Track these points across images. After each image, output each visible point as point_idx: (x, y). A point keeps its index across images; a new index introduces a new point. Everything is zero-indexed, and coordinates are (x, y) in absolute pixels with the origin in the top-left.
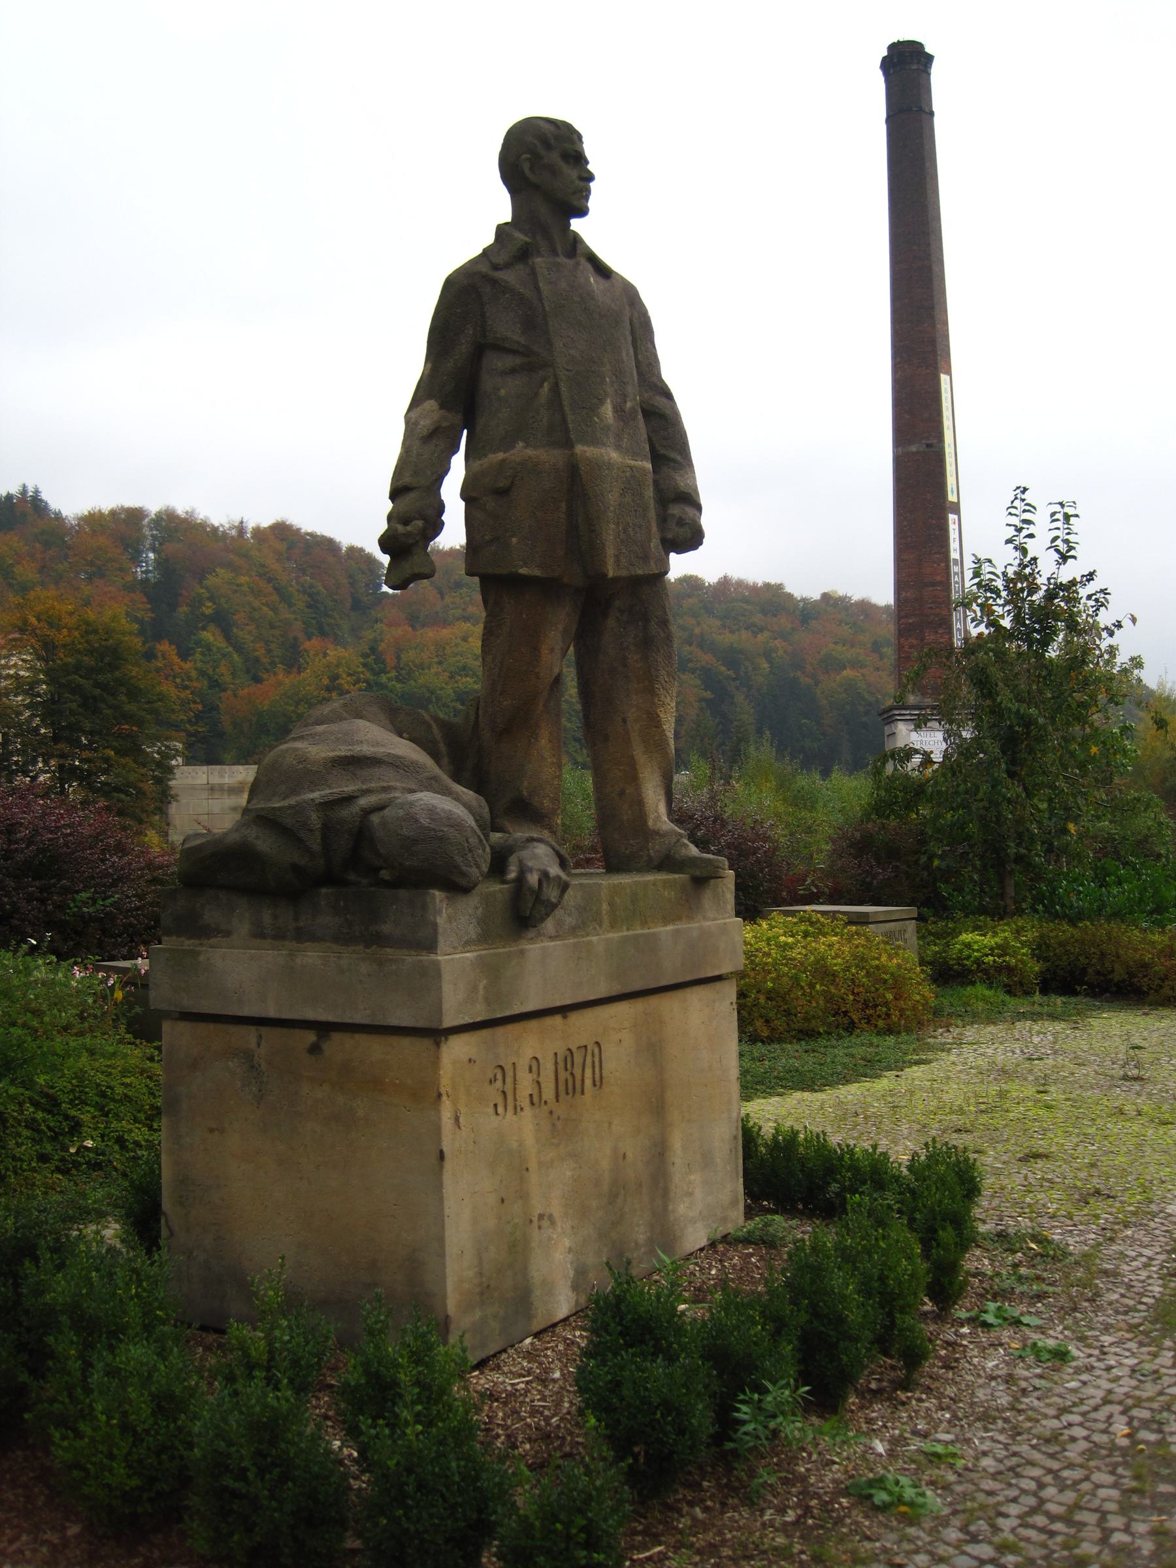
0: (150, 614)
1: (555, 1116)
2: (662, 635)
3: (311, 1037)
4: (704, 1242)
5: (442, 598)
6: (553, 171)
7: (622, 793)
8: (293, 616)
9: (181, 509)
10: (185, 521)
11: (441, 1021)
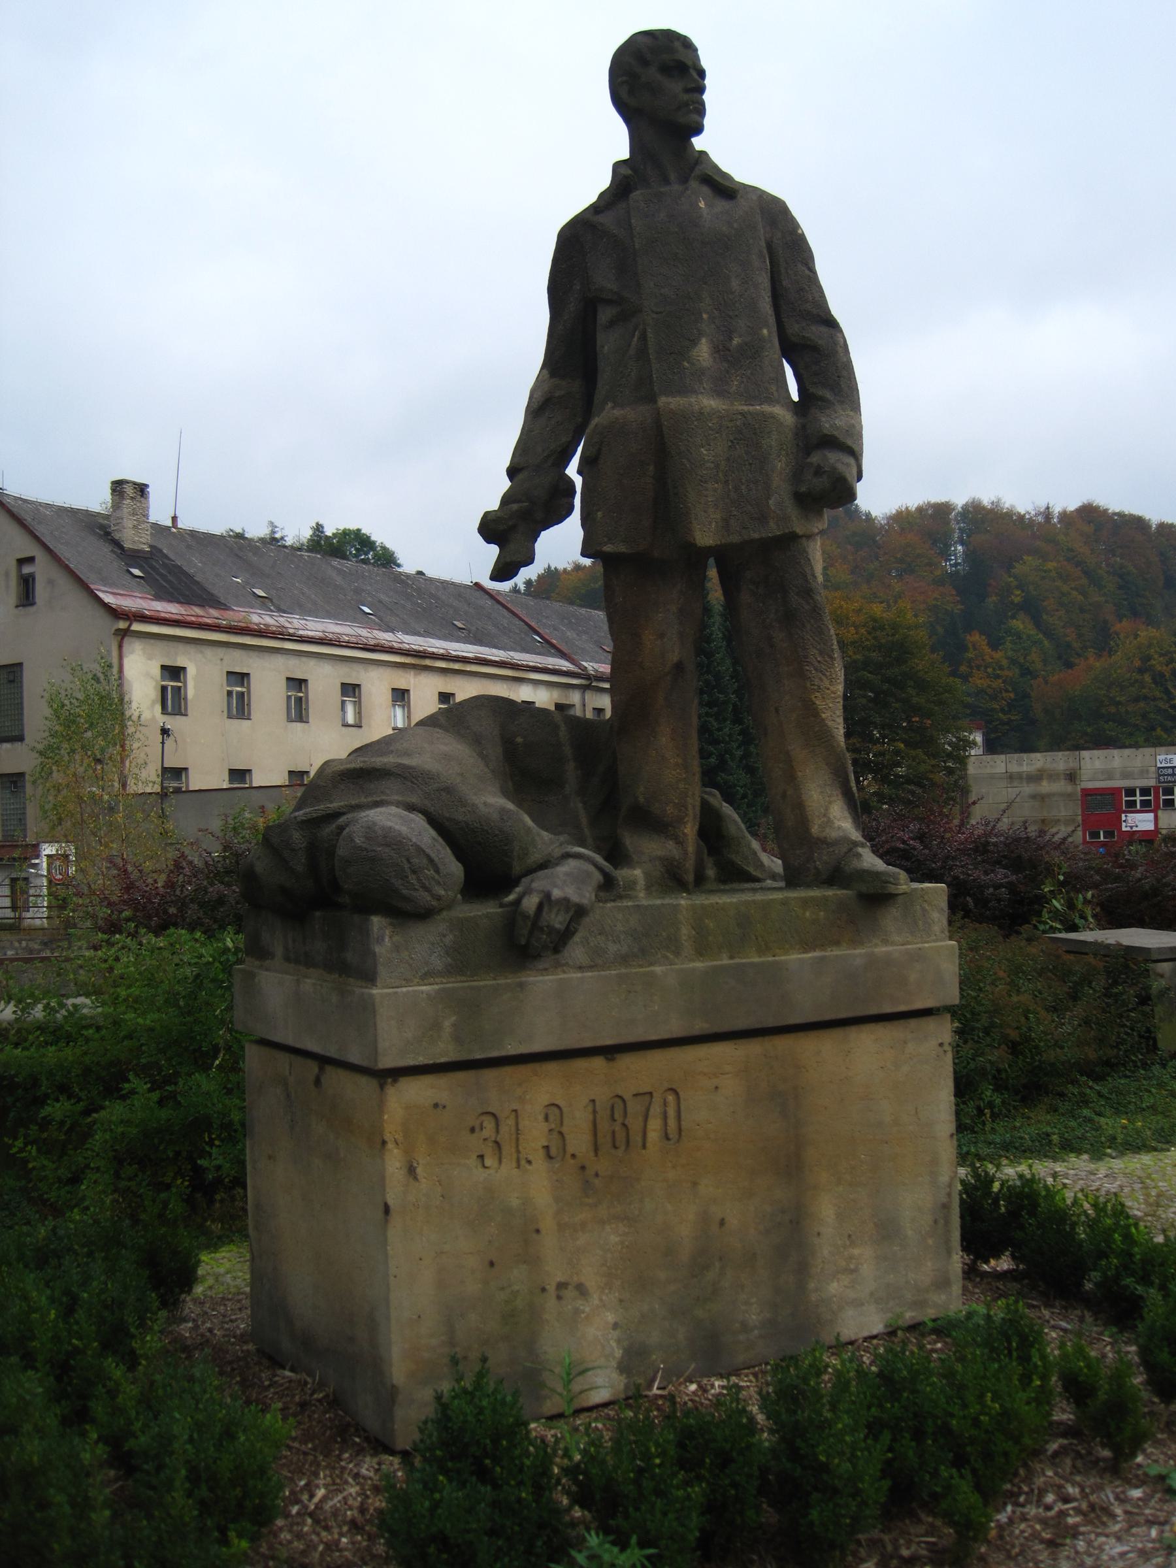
0: (959, 607)
2: (807, 607)
3: (313, 1067)
4: (878, 1328)
7: (784, 795)
8: (1103, 599)
9: (986, 500)
10: (992, 510)
11: (376, 1061)
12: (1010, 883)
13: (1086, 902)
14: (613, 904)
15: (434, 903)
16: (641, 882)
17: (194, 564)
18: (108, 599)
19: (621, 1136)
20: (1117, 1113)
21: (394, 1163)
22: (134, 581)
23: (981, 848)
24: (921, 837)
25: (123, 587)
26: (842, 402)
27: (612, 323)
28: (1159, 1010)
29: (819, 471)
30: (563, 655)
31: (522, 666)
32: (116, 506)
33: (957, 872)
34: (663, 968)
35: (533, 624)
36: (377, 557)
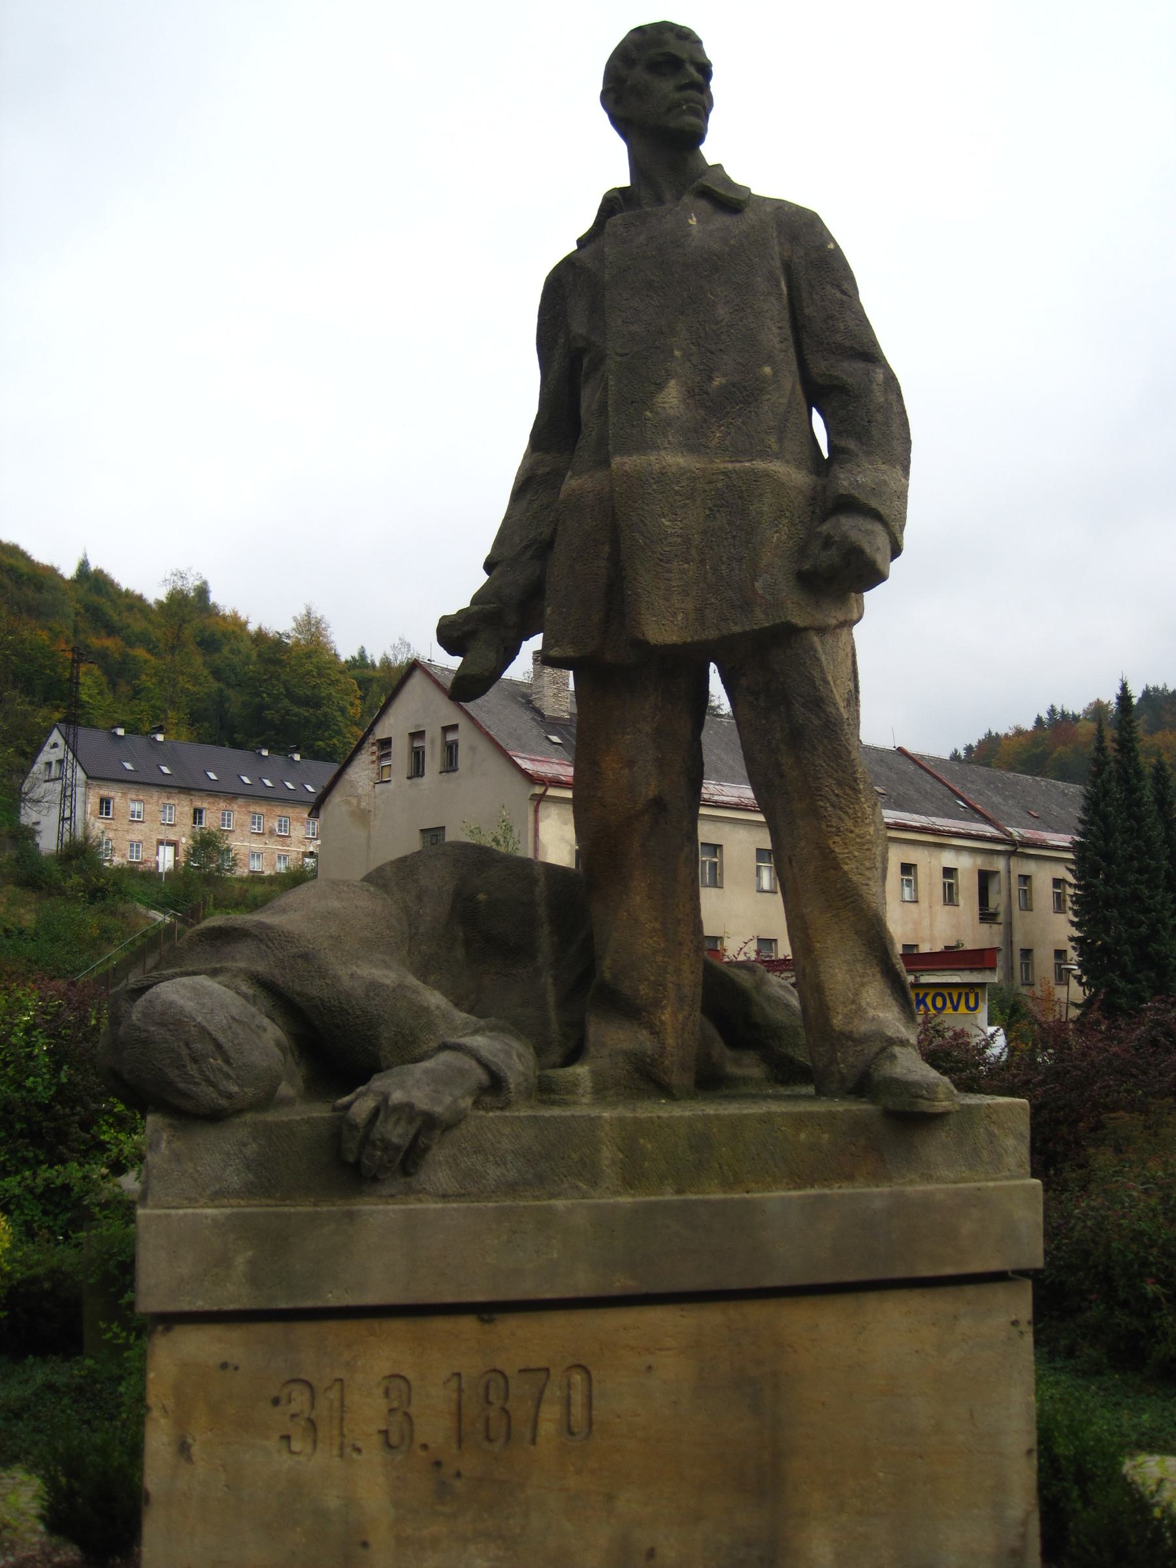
2: (816, 722)
14: (498, 1113)
15: (223, 1102)
18: (525, 765)
22: (552, 748)
25: (541, 753)
26: (869, 453)
29: (828, 543)
31: (944, 831)
34: (569, 1202)
35: (957, 789)
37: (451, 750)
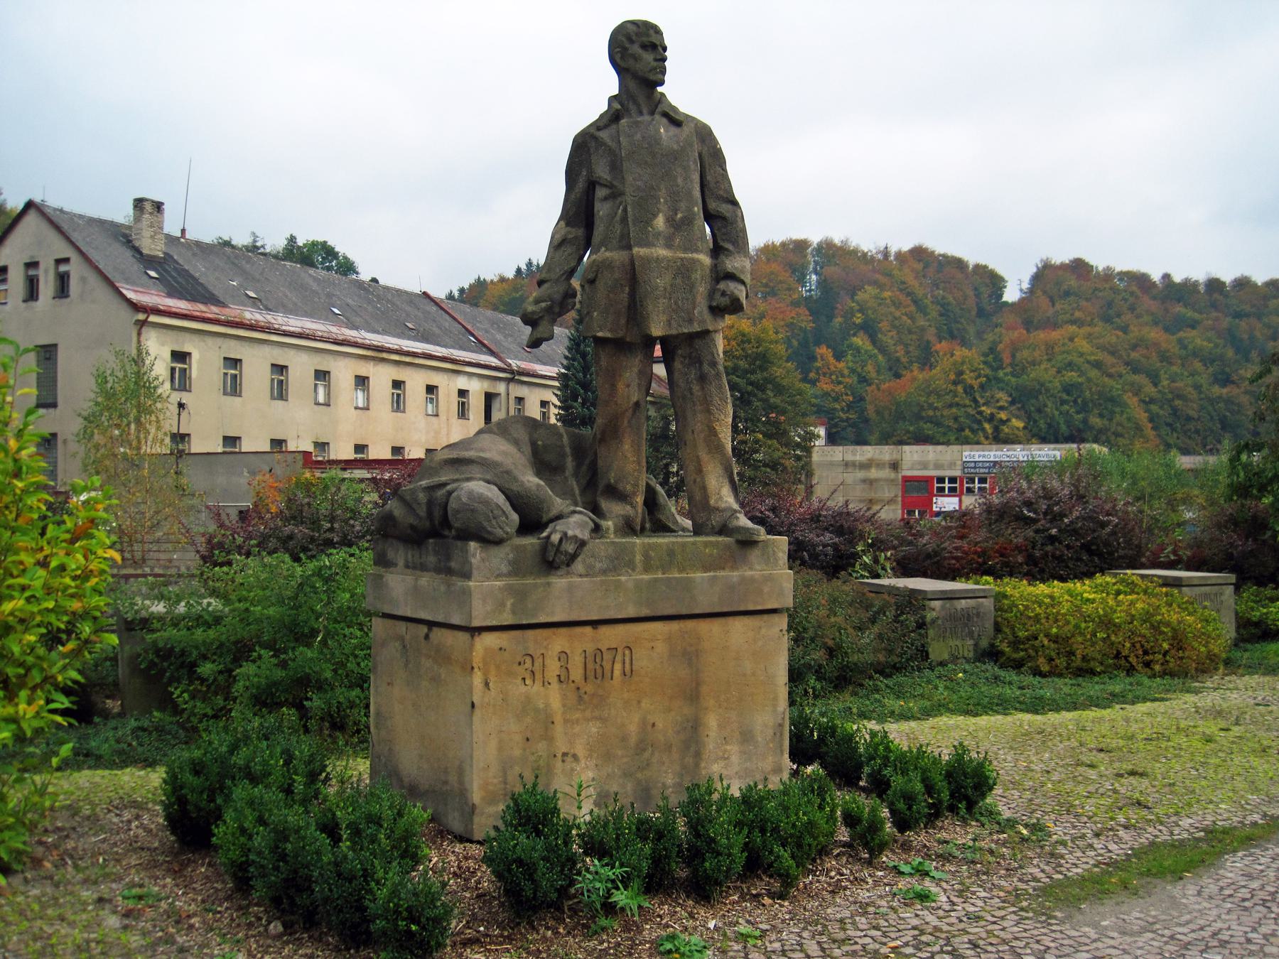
1: (582, 691)
5: (1053, 305)
6: (636, 58)
7: (695, 481)
10: (841, 248)
12: (835, 544)
13: (887, 559)
16: (612, 529)
17: (199, 269)
18: (130, 295)
19: (599, 672)
20: (898, 697)
21: (477, 679)
23: (815, 518)
24: (773, 509)
25: (142, 286)
27: (606, 199)
28: (931, 632)
29: (724, 294)
30: (492, 353)
32: (137, 219)
33: (797, 534)
36: (340, 265)
37: (63, 280)
